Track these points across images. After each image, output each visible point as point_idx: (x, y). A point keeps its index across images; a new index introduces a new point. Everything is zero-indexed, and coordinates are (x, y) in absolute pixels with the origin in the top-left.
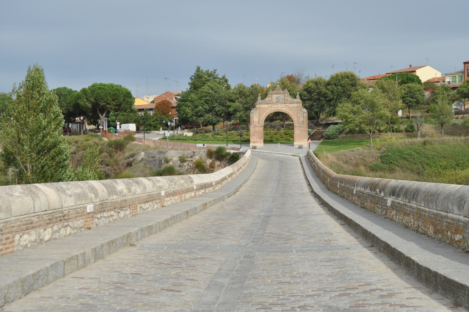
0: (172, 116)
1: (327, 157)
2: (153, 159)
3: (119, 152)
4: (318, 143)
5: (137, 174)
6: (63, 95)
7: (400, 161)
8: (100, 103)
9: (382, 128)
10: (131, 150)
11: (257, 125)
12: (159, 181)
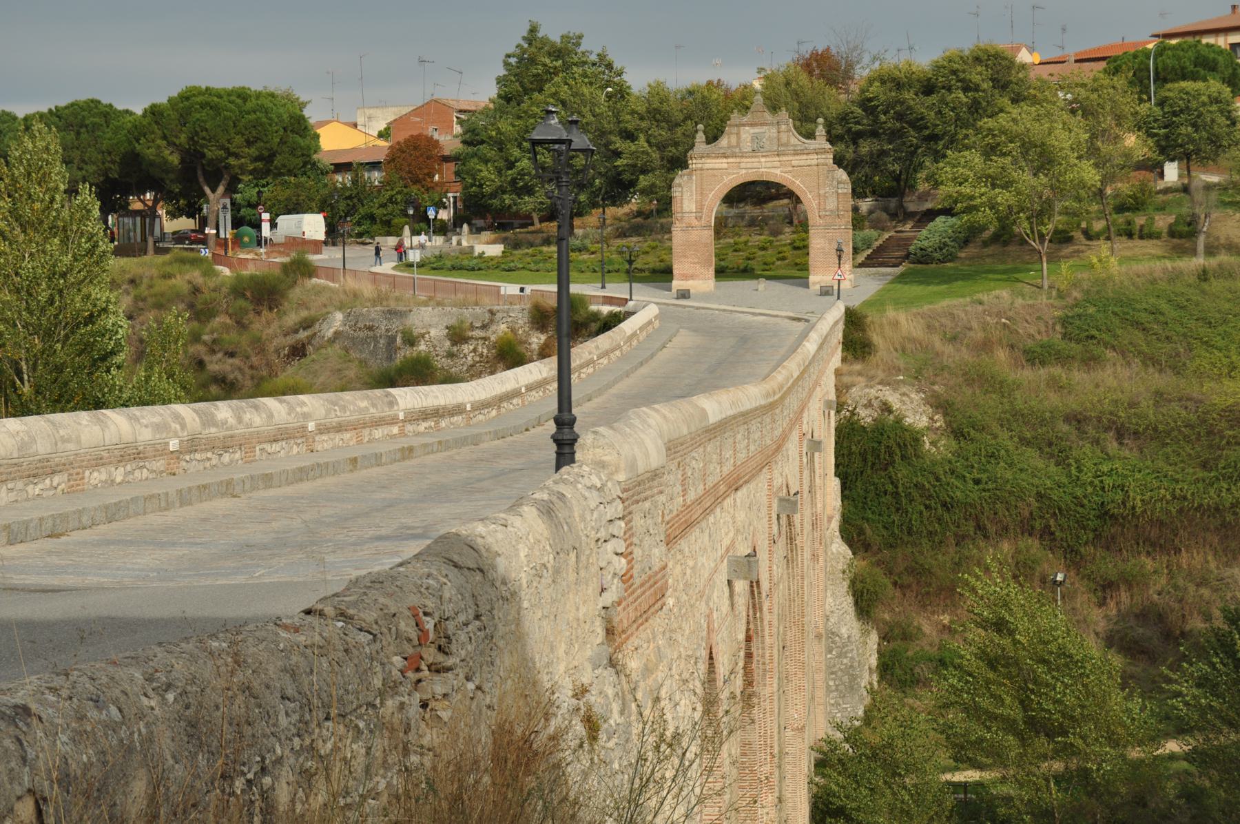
0: (443, 186)
1: (895, 324)
2: (370, 334)
3: (265, 313)
4: (884, 275)
5: (322, 379)
6: (86, 126)
7: (1119, 332)
8: (206, 150)
9: (1099, 226)
10: (303, 305)
11: (695, 223)
12: (303, 404)
